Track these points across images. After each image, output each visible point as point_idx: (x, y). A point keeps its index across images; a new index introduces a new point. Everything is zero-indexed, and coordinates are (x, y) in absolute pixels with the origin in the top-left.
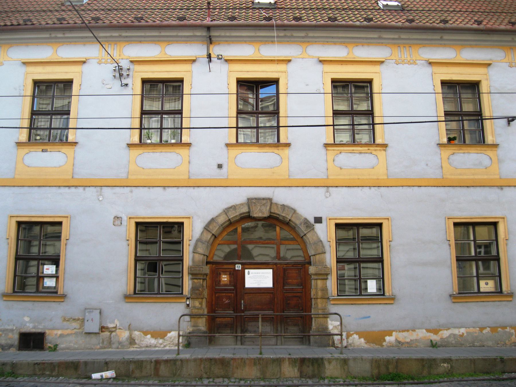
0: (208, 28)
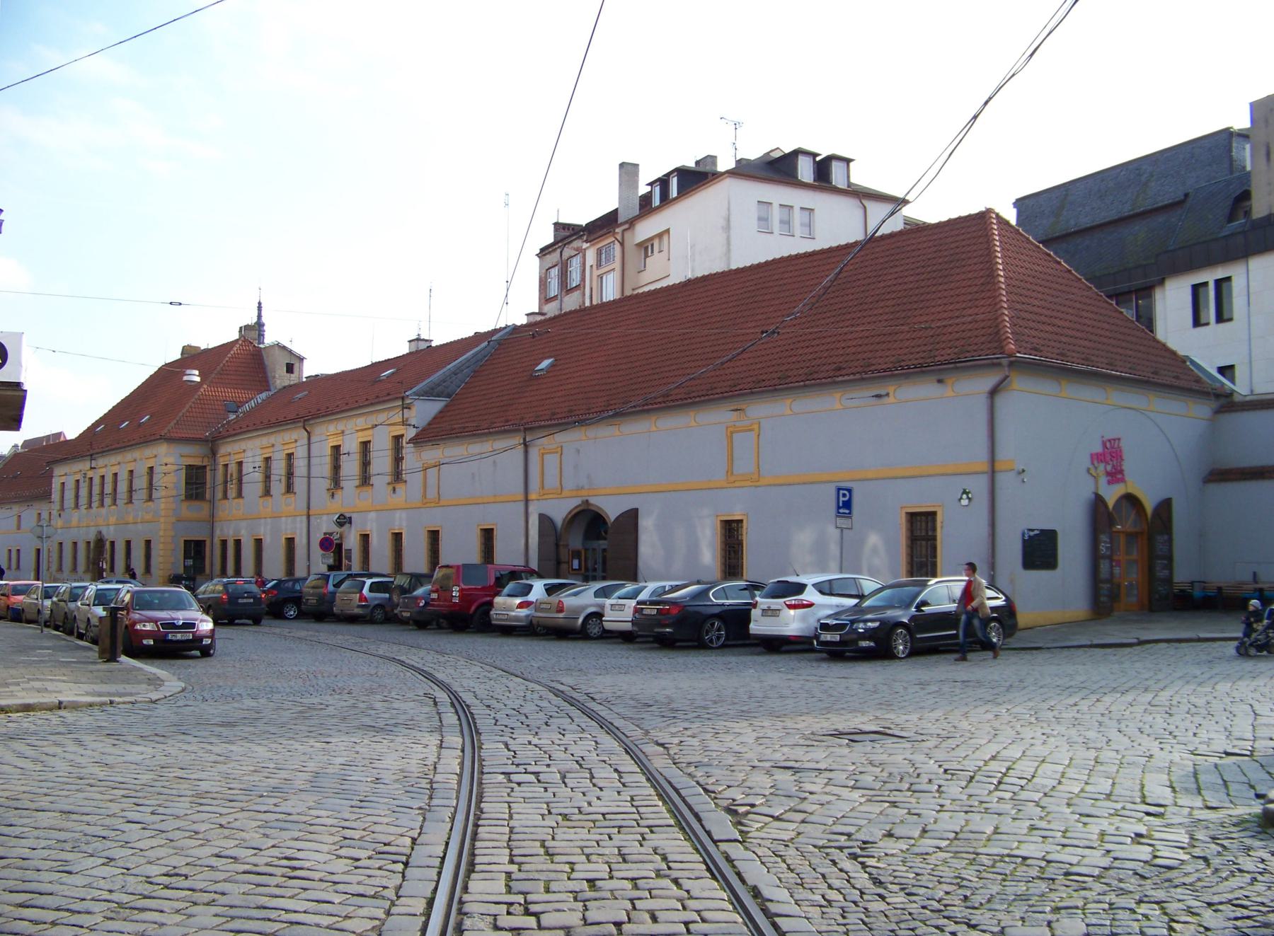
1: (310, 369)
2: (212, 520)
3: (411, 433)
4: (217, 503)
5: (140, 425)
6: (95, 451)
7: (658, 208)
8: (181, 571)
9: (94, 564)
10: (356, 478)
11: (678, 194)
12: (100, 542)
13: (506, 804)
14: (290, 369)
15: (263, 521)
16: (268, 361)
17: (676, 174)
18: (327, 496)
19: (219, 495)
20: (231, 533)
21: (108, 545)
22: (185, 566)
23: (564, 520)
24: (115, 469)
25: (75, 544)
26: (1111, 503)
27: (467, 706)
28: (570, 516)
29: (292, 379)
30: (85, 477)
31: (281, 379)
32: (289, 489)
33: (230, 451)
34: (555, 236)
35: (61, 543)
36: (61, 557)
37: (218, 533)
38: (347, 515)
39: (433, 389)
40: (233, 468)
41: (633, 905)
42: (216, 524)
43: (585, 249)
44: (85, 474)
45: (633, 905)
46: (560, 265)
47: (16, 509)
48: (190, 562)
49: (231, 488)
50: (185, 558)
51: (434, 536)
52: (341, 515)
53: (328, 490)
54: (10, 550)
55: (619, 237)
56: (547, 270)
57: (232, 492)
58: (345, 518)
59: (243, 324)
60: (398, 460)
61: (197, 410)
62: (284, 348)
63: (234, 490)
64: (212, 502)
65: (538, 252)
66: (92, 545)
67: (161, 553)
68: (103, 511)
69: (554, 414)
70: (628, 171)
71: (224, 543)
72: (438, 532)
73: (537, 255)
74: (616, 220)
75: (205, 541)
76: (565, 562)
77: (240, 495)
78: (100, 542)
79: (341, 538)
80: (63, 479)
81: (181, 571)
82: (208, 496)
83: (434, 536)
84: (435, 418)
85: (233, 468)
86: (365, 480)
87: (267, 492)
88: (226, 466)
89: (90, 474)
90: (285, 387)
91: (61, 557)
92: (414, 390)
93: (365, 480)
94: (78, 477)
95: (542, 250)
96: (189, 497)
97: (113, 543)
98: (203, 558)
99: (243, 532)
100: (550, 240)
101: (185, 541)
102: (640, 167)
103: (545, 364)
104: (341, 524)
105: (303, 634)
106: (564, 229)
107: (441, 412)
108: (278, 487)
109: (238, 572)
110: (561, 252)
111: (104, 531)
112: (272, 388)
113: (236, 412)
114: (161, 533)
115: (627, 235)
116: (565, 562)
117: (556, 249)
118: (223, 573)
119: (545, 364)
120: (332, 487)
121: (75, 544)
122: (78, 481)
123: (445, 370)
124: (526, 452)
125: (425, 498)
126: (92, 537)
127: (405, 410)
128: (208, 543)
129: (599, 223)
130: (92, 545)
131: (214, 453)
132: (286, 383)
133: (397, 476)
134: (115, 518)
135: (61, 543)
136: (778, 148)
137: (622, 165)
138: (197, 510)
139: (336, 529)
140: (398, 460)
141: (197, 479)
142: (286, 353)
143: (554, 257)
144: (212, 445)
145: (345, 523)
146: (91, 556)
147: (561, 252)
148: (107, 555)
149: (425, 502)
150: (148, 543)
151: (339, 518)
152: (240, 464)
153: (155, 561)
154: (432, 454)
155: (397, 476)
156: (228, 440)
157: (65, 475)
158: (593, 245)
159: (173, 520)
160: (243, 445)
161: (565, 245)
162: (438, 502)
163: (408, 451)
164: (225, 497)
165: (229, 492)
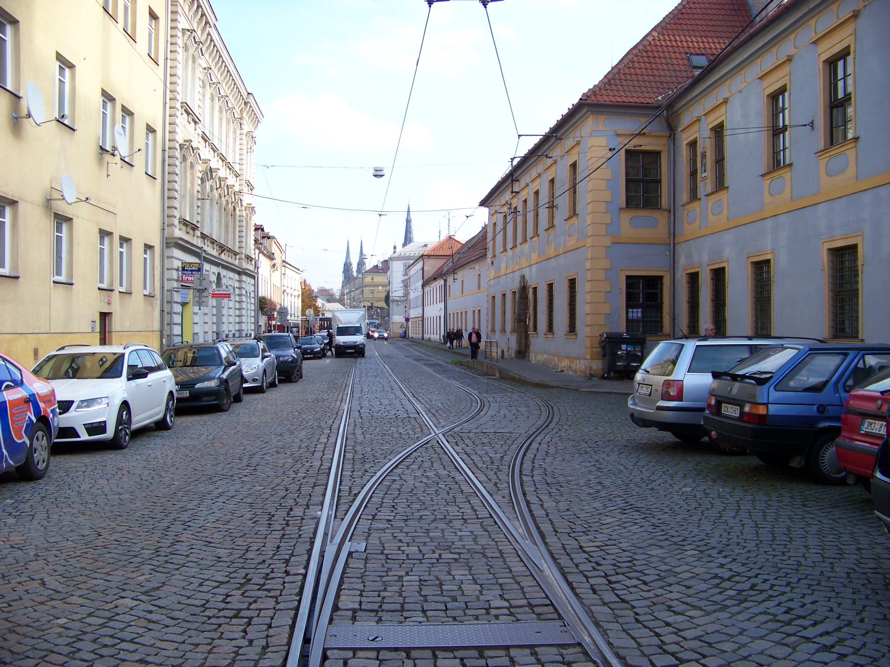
2: (672, 242)
4: (680, 212)
8: (621, 328)
12: (524, 289)
13: (479, 516)
15: (769, 223)
20: (705, 258)
22: (628, 320)
27: (254, 285)
35: (494, 297)
37: (682, 261)
41: (467, 606)
42: (679, 248)
45: (467, 606)
48: (637, 313)
50: (628, 306)
57: (706, 184)
61: (646, 78)
63: (709, 181)
64: (672, 212)
67: (588, 298)
68: (526, 246)
71: (693, 278)
75: (661, 278)
77: (720, 185)
81: (621, 328)
82: (665, 202)
85: (706, 145)
88: (693, 144)
96: (631, 203)
97: (535, 289)
98: (660, 307)
99: (728, 252)
101: (627, 277)
109: (720, 330)
111: (526, 272)
114: (588, 265)
118: (693, 332)
126: (516, 286)
128: (667, 282)
131: (672, 130)
134: (537, 253)
135: (494, 297)
136: (146, 173)
141: (645, 175)
146: (516, 311)
150: (572, 283)
152: (718, 131)
153: (582, 309)
159: (607, 241)
164: (694, 196)
165: (700, 185)
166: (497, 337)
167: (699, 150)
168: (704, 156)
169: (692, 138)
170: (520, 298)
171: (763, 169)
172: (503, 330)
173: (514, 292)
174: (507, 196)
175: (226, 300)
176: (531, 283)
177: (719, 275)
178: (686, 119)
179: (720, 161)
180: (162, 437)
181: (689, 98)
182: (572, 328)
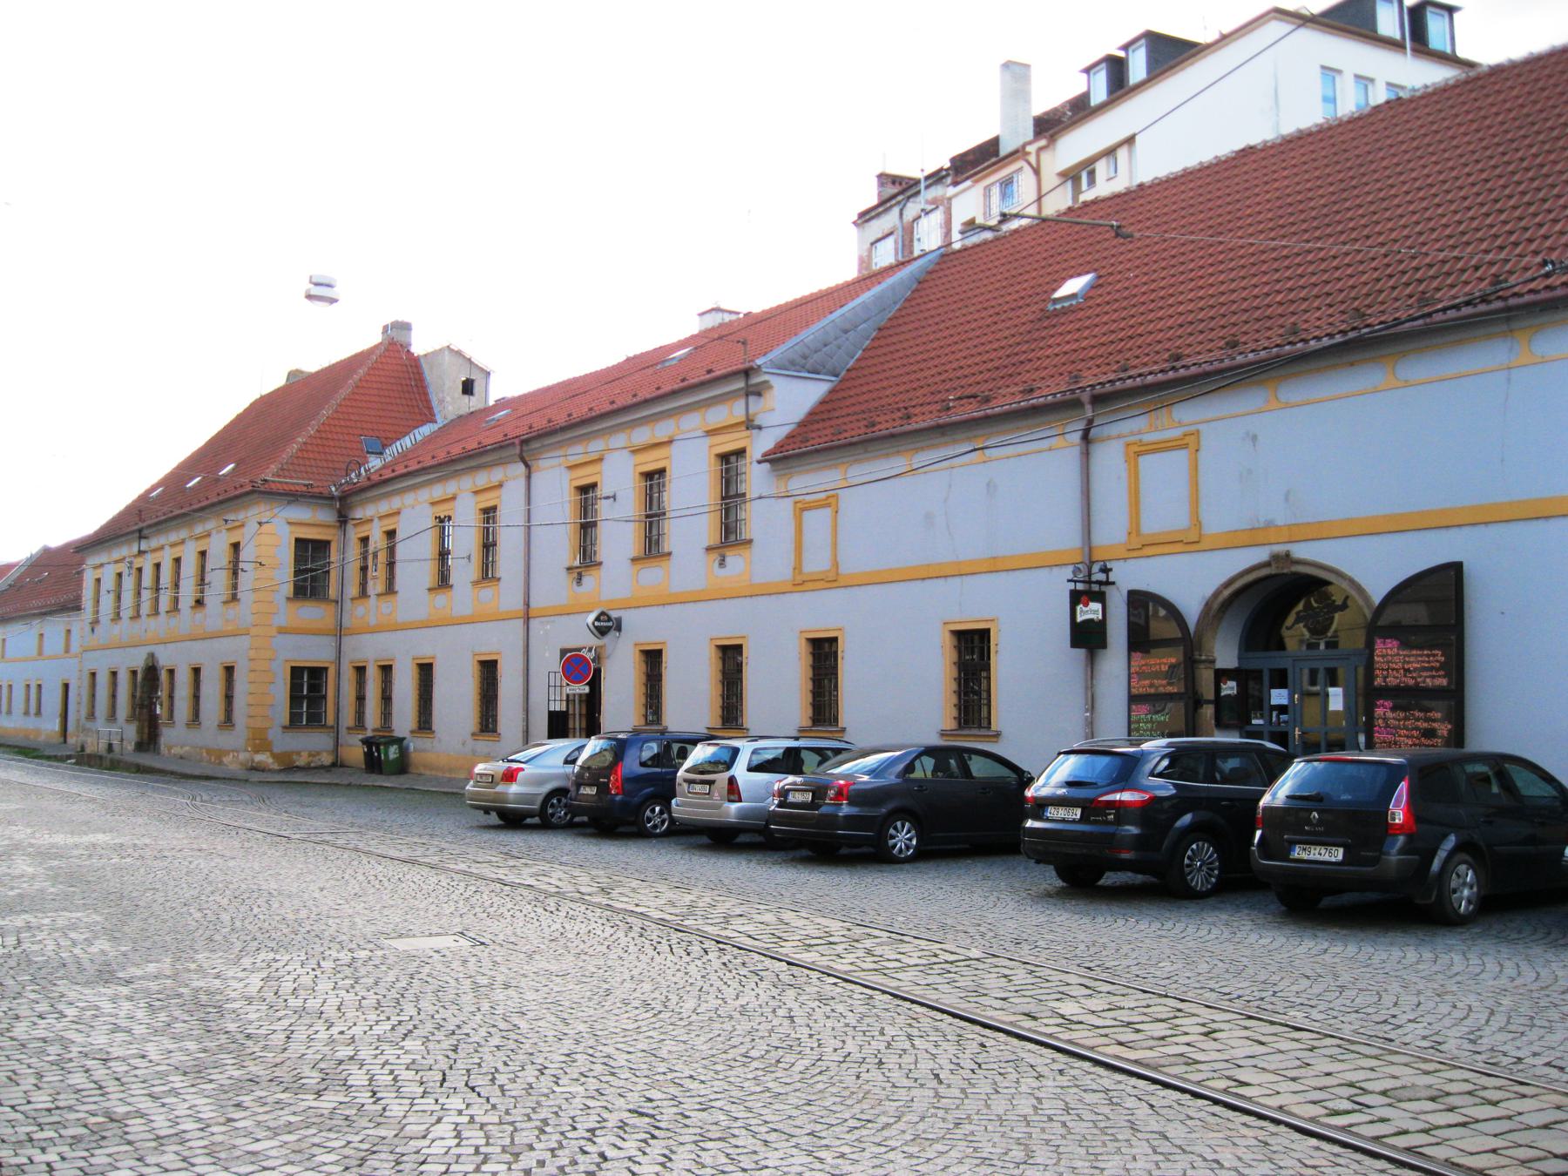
0: (140, 531)
1: (504, 385)
2: (339, 632)
3: (762, 443)
4: (348, 605)
5: (218, 480)
6: (145, 524)
7: (1103, 107)
9: (142, 706)
10: (706, 509)
11: (1149, 71)
12: (152, 671)
14: (468, 388)
16: (429, 376)
17: (1143, 41)
18: (565, 580)
19: (352, 590)
21: (164, 676)
23: (1208, 605)
24: (176, 552)
25: (114, 674)
26: (1192, 608)
28: (1227, 593)
29: (474, 403)
30: (129, 568)
31: (450, 404)
32: (487, 573)
33: (372, 515)
34: (880, 194)
36: (114, 696)
38: (614, 614)
39: (805, 357)
40: (377, 541)
43: (950, 199)
44: (131, 563)
46: (899, 232)
47: (37, 626)
49: (375, 578)
51: (824, 653)
52: (603, 613)
53: (569, 569)
54: (28, 686)
55: (1032, 159)
56: (872, 244)
57: (376, 585)
58: (609, 619)
59: (389, 321)
60: (730, 498)
62: (459, 353)
65: (856, 218)
66: (139, 676)
69: (1178, 358)
70: (1017, 73)
71: (361, 670)
72: (984, 635)
73: (854, 223)
74: (996, 153)
76: (1209, 702)
77: (390, 589)
78: (152, 671)
79: (598, 659)
80: (98, 574)
82: (333, 592)
83: (824, 653)
84: (812, 413)
86: (652, 548)
87: (443, 581)
88: (365, 541)
89: (138, 563)
90: (460, 417)
91: (114, 696)
92: (771, 356)
93: (652, 548)
94: (122, 567)
95: (861, 215)
97: (171, 672)
100: (873, 201)
102: (1032, 69)
103: (1074, 286)
104: (602, 632)
105: (557, 877)
106: (894, 183)
107: (823, 402)
108: (463, 571)
110: (901, 211)
112: (439, 418)
113: (381, 453)
115: (1045, 156)
116: (1209, 702)
117: (892, 207)
119: (1074, 286)
120: (577, 563)
121: (114, 674)
122: (120, 575)
123: (824, 322)
124: (1086, 455)
125: (801, 572)
127: (752, 399)
128: (331, 673)
129: (971, 157)
130: (139, 676)
131: (343, 520)
132: (464, 411)
133: (730, 535)
137: (1007, 65)
138: (313, 613)
139: (592, 641)
140: (730, 498)
142: (461, 361)
143: (890, 220)
144: (343, 506)
145: (609, 628)
146: (138, 694)
147: (901, 211)
148: (162, 693)
149: (802, 583)
151: (598, 619)
154: (811, 481)
155: (730, 535)
156: (369, 494)
157: (100, 571)
158: (977, 181)
160: (396, 503)
161: (909, 198)
162: (832, 580)
163: (755, 478)
164: (364, 593)
165: (370, 583)
166: (100, 724)
167: (371, 549)
168: (375, 555)
169: (391, 528)
170: (144, 679)
171: (224, 598)
172: (112, 716)
173: (134, 673)
174: (125, 551)
175: (284, 624)
176: (165, 659)
177: (386, 670)
178: (358, 513)
179: (391, 565)
180: (441, 401)
181: (390, 488)
182: (228, 720)
